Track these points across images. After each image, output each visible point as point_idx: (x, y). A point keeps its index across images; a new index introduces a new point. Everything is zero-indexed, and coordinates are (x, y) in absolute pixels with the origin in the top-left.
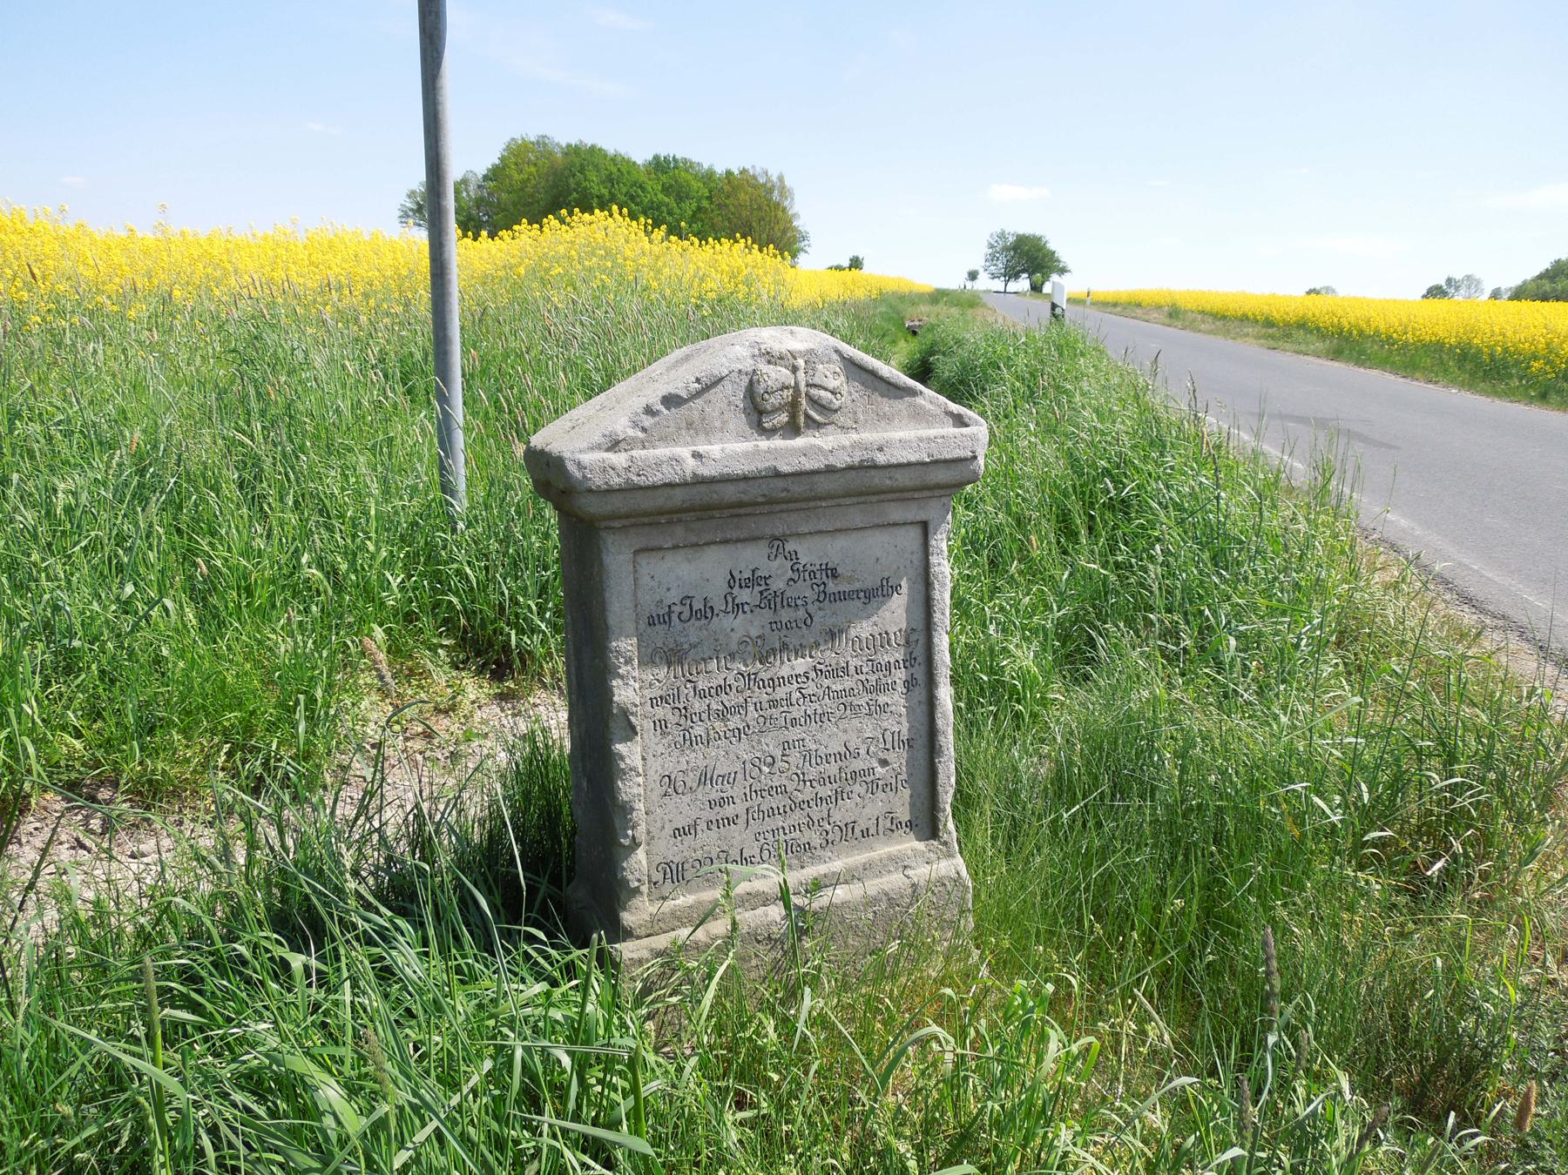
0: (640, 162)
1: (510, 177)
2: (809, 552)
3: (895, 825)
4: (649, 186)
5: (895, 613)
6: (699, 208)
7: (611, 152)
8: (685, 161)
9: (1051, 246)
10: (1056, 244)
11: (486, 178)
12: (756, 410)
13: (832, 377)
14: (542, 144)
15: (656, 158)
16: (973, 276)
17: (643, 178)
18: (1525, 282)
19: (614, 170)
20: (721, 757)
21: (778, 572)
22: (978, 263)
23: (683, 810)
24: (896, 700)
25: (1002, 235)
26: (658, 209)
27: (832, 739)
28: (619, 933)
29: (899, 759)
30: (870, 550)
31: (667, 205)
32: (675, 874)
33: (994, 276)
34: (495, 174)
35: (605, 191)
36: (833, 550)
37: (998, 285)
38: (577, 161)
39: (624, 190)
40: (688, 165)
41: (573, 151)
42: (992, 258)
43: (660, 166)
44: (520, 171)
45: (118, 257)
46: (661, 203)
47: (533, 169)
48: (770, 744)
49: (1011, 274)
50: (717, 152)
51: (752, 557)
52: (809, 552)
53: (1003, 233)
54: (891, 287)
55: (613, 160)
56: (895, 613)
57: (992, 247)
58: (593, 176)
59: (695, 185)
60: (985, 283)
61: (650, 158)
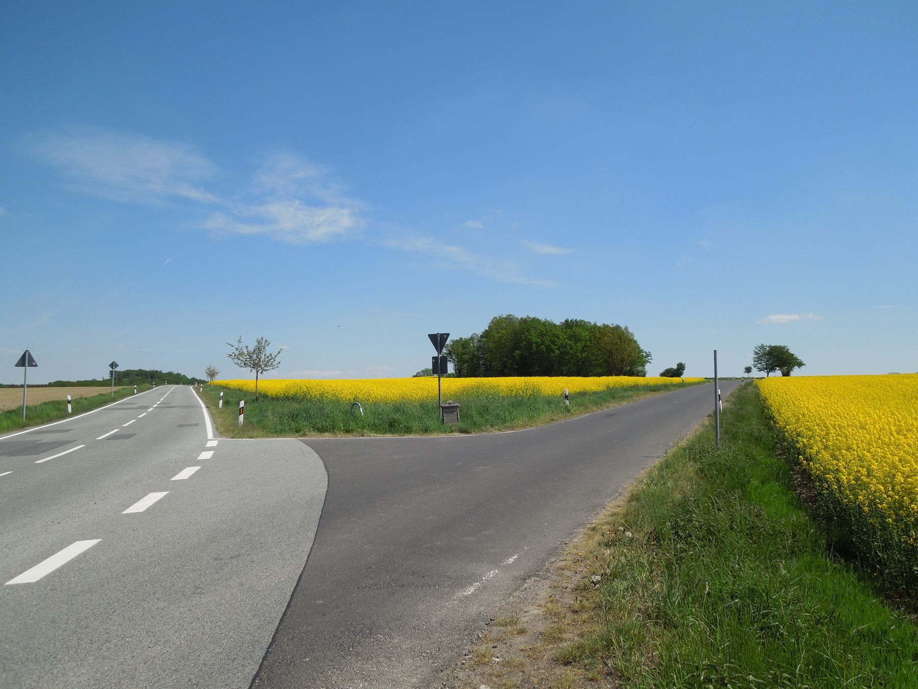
0: (558, 323)
1: (493, 336)
6: (585, 346)
7: (558, 320)
9: (791, 351)
10: (794, 350)
11: (482, 336)
14: (509, 319)
15: (567, 321)
16: (748, 370)
18: (606, 327)
22: (750, 363)
25: (762, 347)
26: (565, 347)
33: (760, 370)
34: (486, 334)
35: (539, 340)
37: (763, 374)
41: (524, 321)
42: (758, 359)
43: (568, 325)
44: (498, 333)
45: (876, 486)
46: (567, 344)
49: (770, 368)
50: (598, 314)
53: (763, 346)
57: (756, 353)
58: (533, 333)
60: (755, 373)
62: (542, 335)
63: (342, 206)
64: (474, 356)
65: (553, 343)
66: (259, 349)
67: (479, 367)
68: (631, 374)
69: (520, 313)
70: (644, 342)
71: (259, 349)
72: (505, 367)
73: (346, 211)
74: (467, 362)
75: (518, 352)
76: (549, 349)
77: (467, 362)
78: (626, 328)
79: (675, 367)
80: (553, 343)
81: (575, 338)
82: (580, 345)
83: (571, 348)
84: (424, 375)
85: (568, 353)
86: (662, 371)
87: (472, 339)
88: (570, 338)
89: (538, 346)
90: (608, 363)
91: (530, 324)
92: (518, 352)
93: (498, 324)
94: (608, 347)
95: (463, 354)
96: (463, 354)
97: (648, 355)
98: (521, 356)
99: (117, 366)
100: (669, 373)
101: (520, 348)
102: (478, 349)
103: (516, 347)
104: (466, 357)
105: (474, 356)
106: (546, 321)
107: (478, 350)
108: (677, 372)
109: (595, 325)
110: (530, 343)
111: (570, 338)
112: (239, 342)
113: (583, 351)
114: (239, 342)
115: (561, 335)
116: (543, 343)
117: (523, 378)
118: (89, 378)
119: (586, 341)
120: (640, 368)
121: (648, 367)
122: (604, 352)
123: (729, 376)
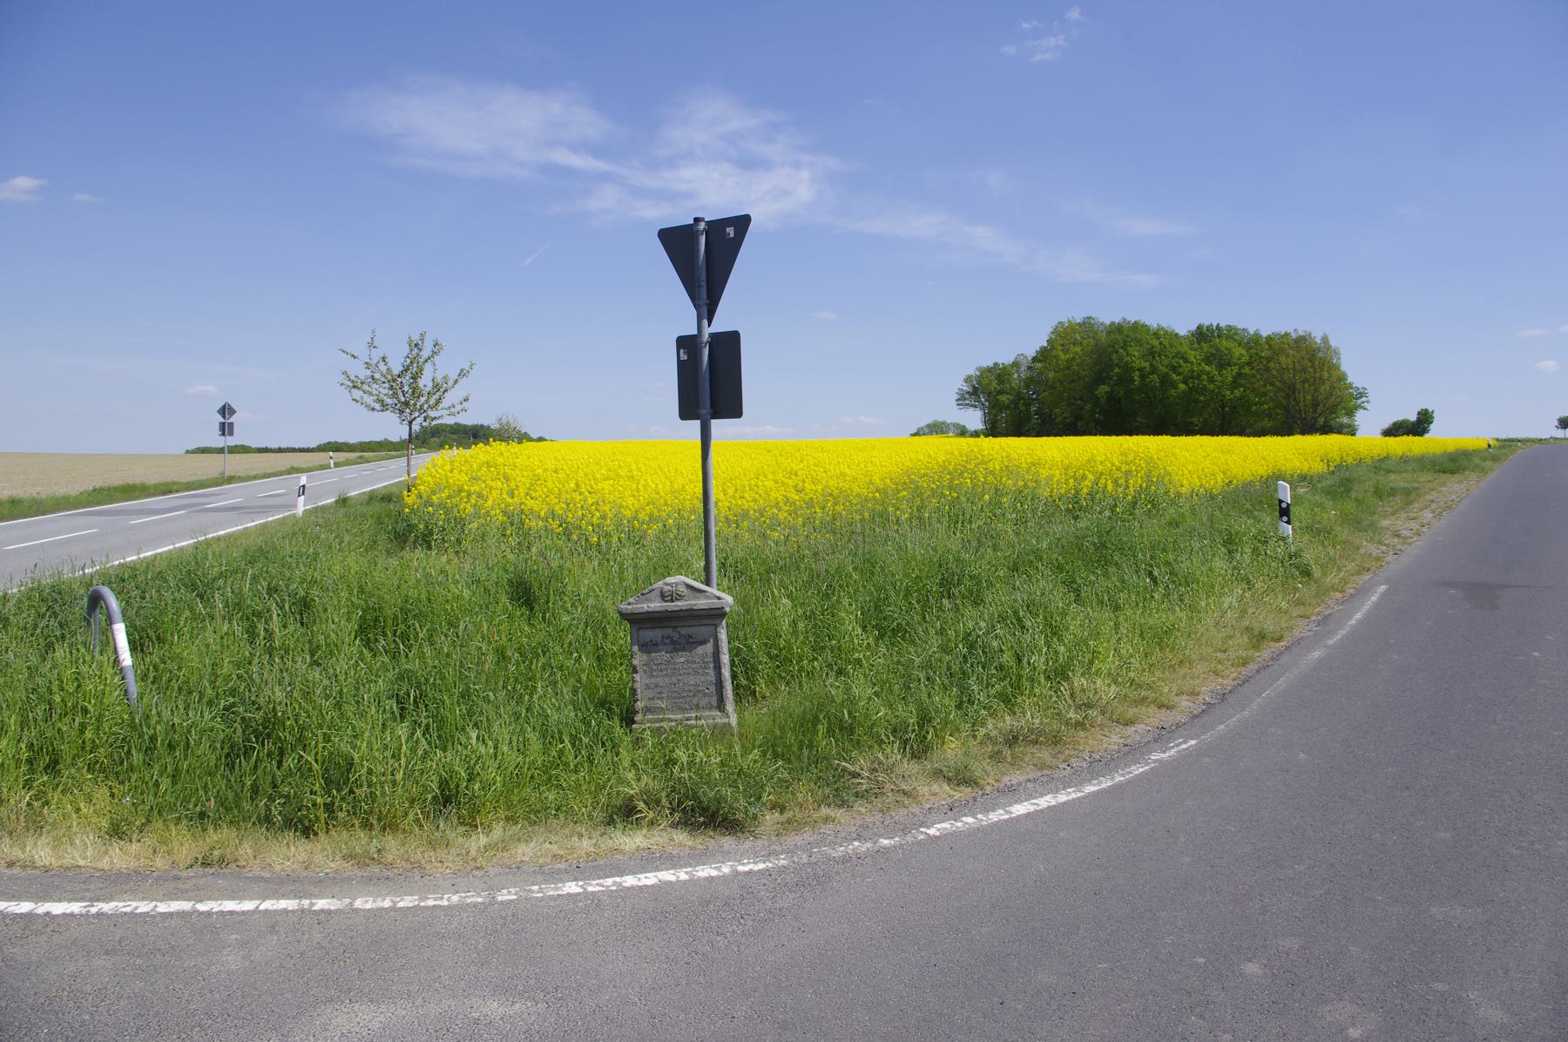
0: (1182, 332)
2: (683, 631)
3: (711, 708)
4: (1192, 355)
5: (709, 647)
6: (1239, 374)
7: (1183, 326)
8: (1229, 328)
11: (1035, 359)
12: (663, 596)
13: (682, 589)
14: (1087, 325)
15: (1199, 327)
17: (1185, 348)
19: (1156, 343)
20: (660, 681)
21: (675, 635)
23: (650, 693)
24: (712, 672)
26: (1199, 377)
27: (692, 680)
28: (634, 722)
29: (712, 688)
30: (700, 631)
31: (1208, 373)
32: (647, 710)
34: (1043, 355)
35: (1146, 365)
36: (690, 631)
38: (1120, 338)
39: (1166, 362)
40: (1231, 333)
41: (1116, 329)
43: (1202, 335)
44: (1066, 351)
47: (1078, 349)
48: (674, 680)
50: (1261, 313)
51: (668, 632)
52: (683, 631)
54: (1451, 448)
55: (1156, 335)
56: (709, 647)
58: (1135, 351)
59: (1238, 352)
61: (1194, 328)
62: (1152, 353)
63: (797, 166)
64: (1019, 396)
65: (1174, 369)
66: (413, 369)
67: (1029, 418)
68: (1326, 430)
69: (1108, 314)
70: (1355, 368)
71: (413, 369)
72: (1078, 417)
73: (805, 175)
74: (1008, 407)
75: (1103, 389)
76: (1166, 382)
77: (1008, 407)
78: (1325, 339)
79: (1413, 418)
80: (1174, 369)
81: (1220, 360)
82: (1229, 374)
83: (1211, 380)
84: (931, 433)
85: (1204, 389)
86: (1386, 425)
87: (1016, 364)
88: (1208, 360)
89: (1143, 377)
90: (1286, 409)
91: (1126, 334)
92: (1103, 389)
93: (1064, 336)
94: (1288, 376)
95: (1001, 392)
96: (1001, 392)
97: (1361, 395)
98: (1111, 397)
99: (232, 412)
100: (1395, 430)
101: (1099, 384)
102: (1029, 382)
103: (1100, 379)
104: (1004, 398)
105: (1019, 396)
106: (1160, 328)
107: (1027, 387)
108: (1420, 426)
109: (1257, 335)
110: (1128, 369)
111: (1208, 360)
112: (372, 345)
113: (1235, 384)
114: (372, 345)
115: (1192, 356)
116: (1154, 370)
117: (1114, 438)
118: (263, 446)
119: (1242, 367)
120: (1345, 420)
121: (1360, 418)
122: (1282, 388)
123: (1533, 436)
